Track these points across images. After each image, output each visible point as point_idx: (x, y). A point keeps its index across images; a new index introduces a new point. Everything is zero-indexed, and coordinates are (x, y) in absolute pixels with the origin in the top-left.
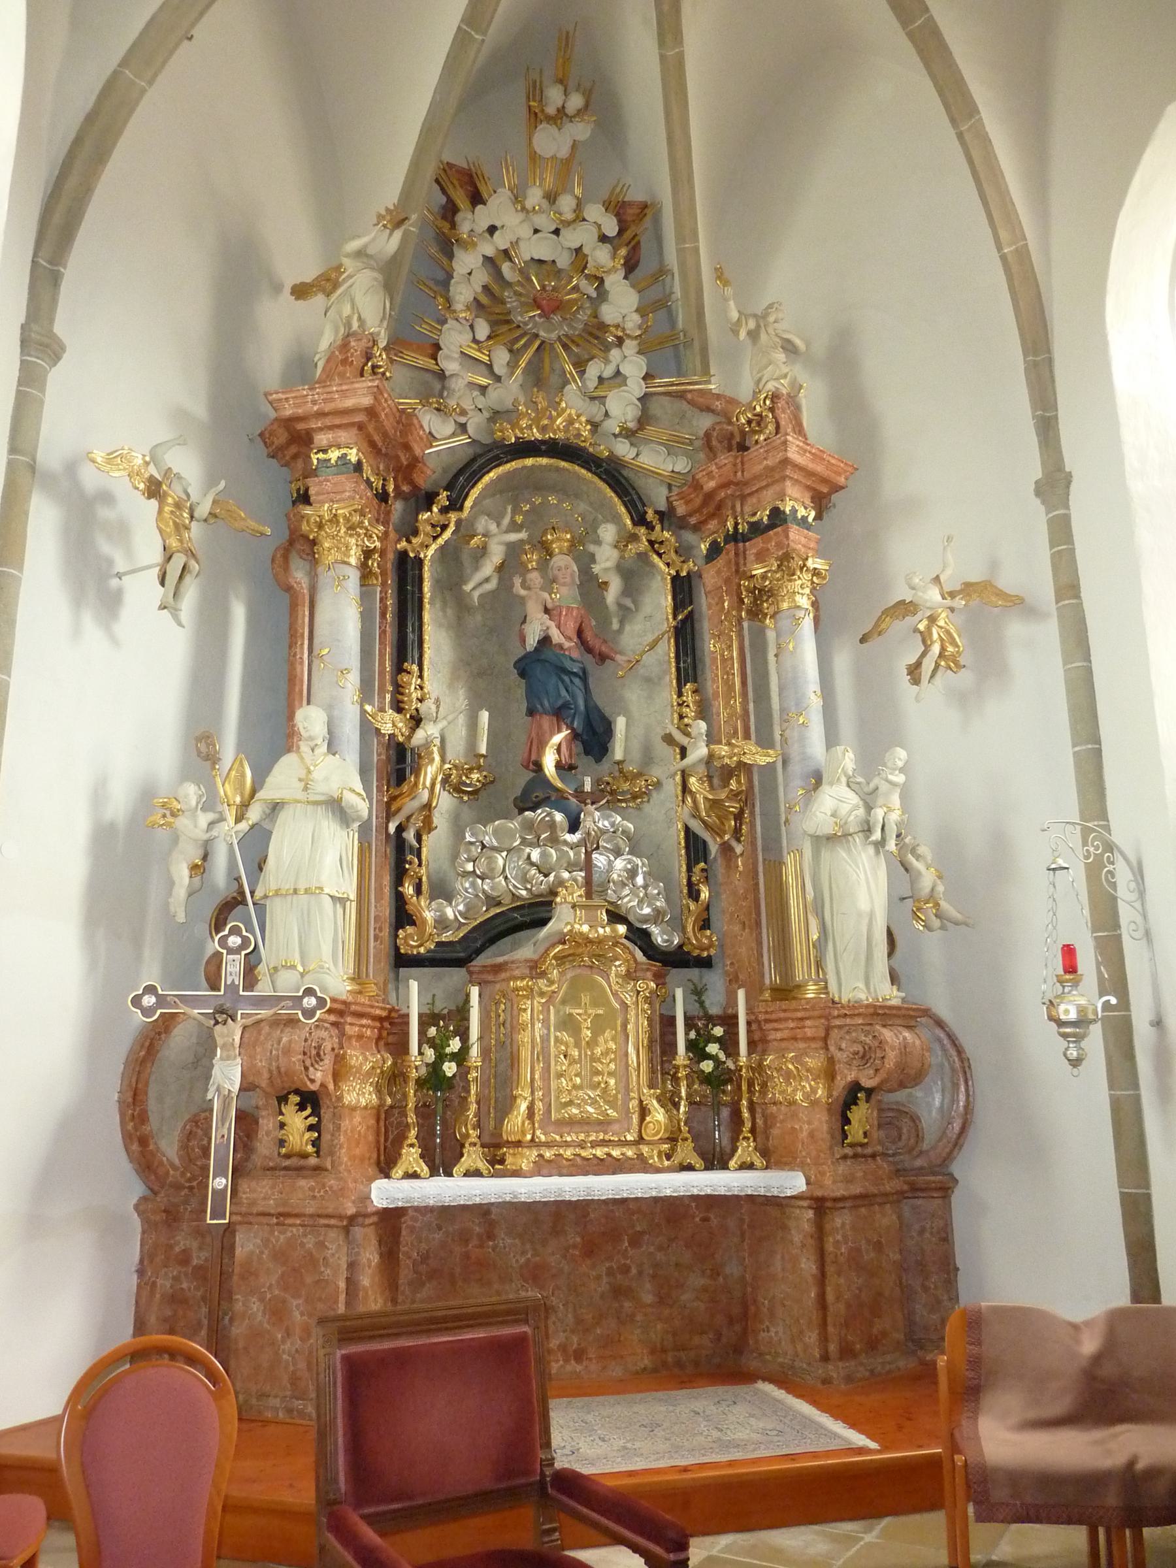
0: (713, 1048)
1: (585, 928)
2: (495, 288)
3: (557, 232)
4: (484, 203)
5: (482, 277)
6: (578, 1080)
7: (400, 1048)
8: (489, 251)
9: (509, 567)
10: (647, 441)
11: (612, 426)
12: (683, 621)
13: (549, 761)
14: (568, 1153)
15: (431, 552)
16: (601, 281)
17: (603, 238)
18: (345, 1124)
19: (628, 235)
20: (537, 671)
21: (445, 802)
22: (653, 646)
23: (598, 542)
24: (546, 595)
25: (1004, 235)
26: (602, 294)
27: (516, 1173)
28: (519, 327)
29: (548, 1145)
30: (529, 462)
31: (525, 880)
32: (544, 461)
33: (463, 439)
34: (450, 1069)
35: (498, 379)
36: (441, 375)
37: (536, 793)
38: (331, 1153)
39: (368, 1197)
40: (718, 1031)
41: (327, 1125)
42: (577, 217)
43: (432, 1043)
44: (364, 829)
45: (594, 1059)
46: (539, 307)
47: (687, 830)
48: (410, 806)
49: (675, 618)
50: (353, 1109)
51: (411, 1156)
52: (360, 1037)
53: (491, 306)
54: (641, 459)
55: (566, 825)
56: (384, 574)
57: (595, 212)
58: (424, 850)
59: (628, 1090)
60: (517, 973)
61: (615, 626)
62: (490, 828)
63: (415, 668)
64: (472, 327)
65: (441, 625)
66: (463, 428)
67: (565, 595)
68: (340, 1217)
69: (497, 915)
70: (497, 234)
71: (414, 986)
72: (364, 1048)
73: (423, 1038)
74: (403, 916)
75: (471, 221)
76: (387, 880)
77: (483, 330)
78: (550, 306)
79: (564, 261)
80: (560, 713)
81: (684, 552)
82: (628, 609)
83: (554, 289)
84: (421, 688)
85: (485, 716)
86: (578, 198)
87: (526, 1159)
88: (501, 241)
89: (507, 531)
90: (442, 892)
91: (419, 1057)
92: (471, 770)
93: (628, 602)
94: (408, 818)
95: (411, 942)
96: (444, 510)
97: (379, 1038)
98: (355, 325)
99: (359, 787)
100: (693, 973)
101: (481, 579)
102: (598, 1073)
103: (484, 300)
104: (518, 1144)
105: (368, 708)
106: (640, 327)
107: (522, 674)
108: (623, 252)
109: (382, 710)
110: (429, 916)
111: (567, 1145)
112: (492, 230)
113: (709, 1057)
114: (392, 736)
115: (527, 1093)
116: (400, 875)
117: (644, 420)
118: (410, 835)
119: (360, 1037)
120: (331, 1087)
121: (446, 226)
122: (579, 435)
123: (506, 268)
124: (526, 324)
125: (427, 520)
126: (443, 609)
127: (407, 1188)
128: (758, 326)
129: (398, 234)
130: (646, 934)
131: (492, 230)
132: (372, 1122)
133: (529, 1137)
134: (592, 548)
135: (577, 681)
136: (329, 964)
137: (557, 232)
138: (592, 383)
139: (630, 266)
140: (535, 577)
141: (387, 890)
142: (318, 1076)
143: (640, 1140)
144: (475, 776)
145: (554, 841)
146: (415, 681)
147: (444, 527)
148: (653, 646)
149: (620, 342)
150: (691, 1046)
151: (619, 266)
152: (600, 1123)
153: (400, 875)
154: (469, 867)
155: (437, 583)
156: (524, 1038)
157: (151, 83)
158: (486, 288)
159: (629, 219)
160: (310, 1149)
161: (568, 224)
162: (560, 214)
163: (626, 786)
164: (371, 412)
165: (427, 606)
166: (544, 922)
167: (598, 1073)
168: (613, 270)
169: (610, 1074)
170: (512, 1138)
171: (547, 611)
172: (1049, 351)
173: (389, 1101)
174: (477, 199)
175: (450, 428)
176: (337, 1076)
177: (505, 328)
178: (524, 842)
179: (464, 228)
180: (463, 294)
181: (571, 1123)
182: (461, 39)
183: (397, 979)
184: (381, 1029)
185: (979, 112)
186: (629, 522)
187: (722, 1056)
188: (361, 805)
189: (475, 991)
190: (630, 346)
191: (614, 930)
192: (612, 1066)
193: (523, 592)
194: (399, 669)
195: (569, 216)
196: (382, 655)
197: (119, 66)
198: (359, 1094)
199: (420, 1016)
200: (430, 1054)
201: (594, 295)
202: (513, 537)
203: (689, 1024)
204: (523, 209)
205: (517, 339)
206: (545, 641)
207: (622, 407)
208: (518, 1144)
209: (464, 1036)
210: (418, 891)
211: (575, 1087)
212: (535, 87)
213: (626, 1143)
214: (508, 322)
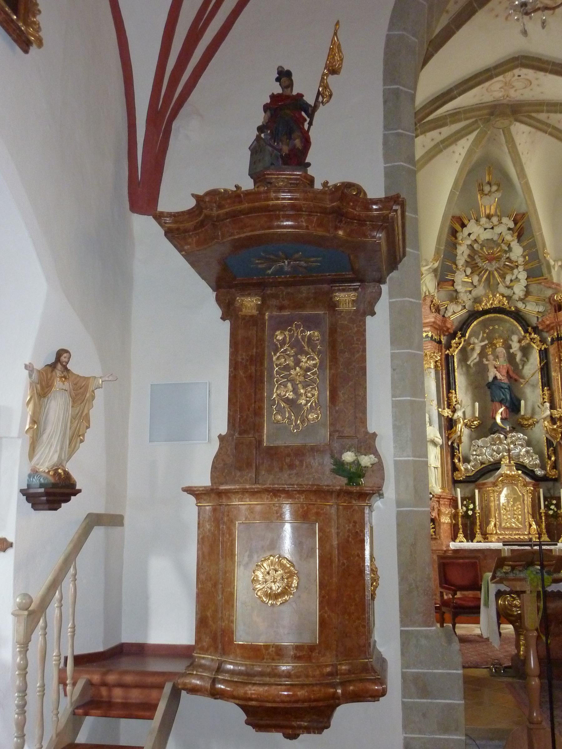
0: (552, 507)
1: (508, 472)
3: (492, 228)
5: (467, 252)
6: (509, 517)
7: (456, 507)
8: (469, 242)
9: (483, 354)
10: (529, 301)
11: (516, 297)
12: (543, 366)
13: (498, 420)
14: (507, 537)
15: (456, 353)
16: (510, 244)
18: (442, 527)
19: (518, 225)
20: (493, 387)
21: (466, 431)
22: (534, 374)
23: (511, 340)
24: (495, 362)
26: (510, 249)
27: (491, 542)
29: (501, 534)
30: (487, 316)
31: (492, 456)
32: (492, 315)
33: (465, 311)
34: (470, 513)
35: (475, 287)
36: (456, 291)
37: (494, 429)
38: (439, 534)
39: (449, 546)
40: (554, 502)
41: (437, 528)
43: (465, 506)
44: (441, 447)
45: (514, 510)
46: (487, 260)
47: (547, 438)
48: (454, 436)
49: (540, 364)
50: (444, 523)
51: (461, 536)
52: (444, 504)
53: (473, 253)
54: (527, 308)
55: (504, 438)
56: (442, 366)
58: (460, 448)
59: (525, 519)
60: (489, 485)
61: (521, 367)
62: (480, 440)
63: (453, 391)
64: (465, 271)
65: (461, 374)
66: (464, 307)
67: (502, 362)
68: (442, 550)
69: (484, 467)
70: (471, 236)
71: (459, 490)
72: (446, 507)
73: (462, 505)
74: (455, 468)
75: (462, 234)
76: (449, 458)
77: (469, 271)
78: (491, 259)
79: (495, 238)
80: (502, 402)
81: (543, 341)
82: (525, 361)
83: (492, 253)
84: (456, 397)
85: (477, 404)
87: (494, 538)
88: (473, 237)
89: (481, 342)
90: (466, 460)
91: (461, 510)
92: (473, 421)
93: (525, 359)
94: (454, 440)
95: (459, 476)
96: (460, 338)
97: (450, 504)
98: (427, 294)
99: (439, 435)
100: (550, 484)
101: (474, 357)
102: (515, 514)
103: (469, 260)
104: (492, 534)
105: (440, 410)
107: (489, 388)
108: (516, 234)
109: (444, 409)
110: (462, 468)
111: (506, 535)
113: (551, 509)
114: (448, 416)
115: (494, 520)
116: (453, 456)
117: (528, 293)
118: (455, 445)
119: (444, 504)
120: (437, 517)
122: (504, 304)
123: (476, 246)
125: (455, 343)
126: (462, 368)
127: (461, 544)
130: (533, 471)
132: (449, 527)
133: (495, 532)
134: (510, 342)
135: (506, 390)
136: (434, 485)
137: (492, 228)
138: (508, 283)
140: (491, 357)
141: (449, 461)
142: (434, 514)
143: (529, 533)
144: (475, 423)
145: (501, 443)
146: (454, 395)
147: (460, 344)
148: (534, 374)
149: (517, 266)
150: (546, 506)
152: (516, 528)
153: (453, 456)
154: (475, 453)
155: (460, 361)
156: (492, 504)
160: (433, 534)
161: (496, 225)
163: (526, 423)
164: (434, 322)
165: (456, 370)
166: (498, 469)
167: (515, 514)
168: (513, 240)
169: (519, 515)
170: (490, 532)
171: (495, 368)
173: (454, 522)
174: (463, 226)
175: (460, 308)
176: (439, 515)
177: (476, 268)
178: (491, 444)
179: (460, 238)
180: (461, 260)
181: (508, 529)
183: (454, 486)
184: (450, 502)
186: (522, 332)
187: (555, 509)
188: (439, 441)
189: (477, 491)
190: (521, 268)
191: (517, 472)
192: (520, 512)
193: (487, 363)
194: (448, 392)
196: (442, 374)
198: (445, 520)
199: (461, 497)
200: (464, 508)
202: (483, 344)
203: (545, 499)
205: (481, 272)
206: (495, 378)
207: (519, 290)
208: (492, 534)
209: (474, 503)
210: (459, 461)
211: (508, 518)
213: (525, 534)
214: (478, 266)
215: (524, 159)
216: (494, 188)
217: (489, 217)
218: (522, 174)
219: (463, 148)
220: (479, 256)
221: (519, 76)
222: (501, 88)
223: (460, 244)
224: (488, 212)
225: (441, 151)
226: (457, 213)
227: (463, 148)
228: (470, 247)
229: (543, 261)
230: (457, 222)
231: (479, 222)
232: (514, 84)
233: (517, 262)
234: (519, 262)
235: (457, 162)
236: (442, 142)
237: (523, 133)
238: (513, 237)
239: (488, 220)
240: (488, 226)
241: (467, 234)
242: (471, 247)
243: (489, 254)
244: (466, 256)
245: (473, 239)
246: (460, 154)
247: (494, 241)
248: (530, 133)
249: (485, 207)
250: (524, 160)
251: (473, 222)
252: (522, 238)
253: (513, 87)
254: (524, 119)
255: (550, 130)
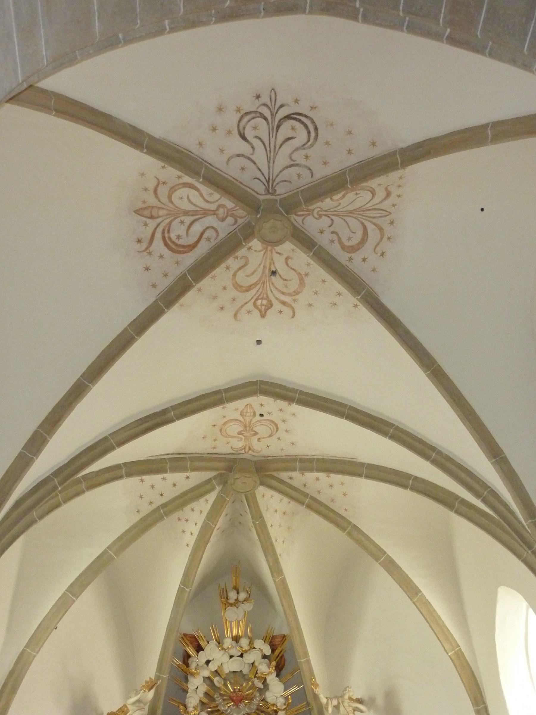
2: (211, 692)
3: (241, 656)
4: (203, 650)
5: (203, 688)
8: (206, 674)
16: (265, 680)
17: (264, 657)
19: (277, 652)
25: (447, 646)
28: (223, 713)
42: (251, 647)
46: (233, 701)
57: (259, 644)
70: (211, 663)
79: (246, 671)
83: (240, 691)
86: (249, 638)
88: (213, 667)
103: (205, 701)
106: (285, 704)
108: (274, 663)
112: (208, 662)
121: (184, 666)
123: (216, 680)
124: (226, 711)
128: (339, 703)
129: (152, 692)
131: (208, 662)
137: (241, 656)
139: (279, 669)
151: (273, 671)
157: (37, 653)
158: (206, 694)
159: (277, 643)
161: (246, 651)
162: (242, 647)
168: (269, 673)
172: (484, 703)
174: (199, 649)
179: (193, 666)
182: (181, 591)
185: (421, 591)
195: (246, 648)
197: (25, 647)
201: (262, 686)
204: (223, 649)
212: (223, 592)
214: (219, 710)
215: (279, 548)
216: (243, 596)
217: (236, 639)
218: (276, 569)
219: (196, 524)
220: (221, 695)
221: (262, 415)
222: (240, 433)
223: (192, 674)
224: (235, 632)
225: (161, 518)
226: (188, 628)
227: (196, 524)
228: (208, 682)
229: (313, 703)
230: (191, 643)
231: (223, 644)
232: (256, 429)
233: (274, 705)
234: (279, 705)
235: (188, 545)
236: (164, 506)
237: (276, 511)
238: (269, 668)
239: (234, 643)
240: (236, 652)
241: (204, 661)
242: (208, 680)
243: (234, 691)
244: (201, 694)
245: (214, 670)
246: (192, 534)
247: (244, 676)
248: (284, 513)
249: (231, 623)
250: (278, 551)
251: (213, 643)
252: (283, 672)
253: (256, 433)
254: (274, 483)
255: (307, 501)
